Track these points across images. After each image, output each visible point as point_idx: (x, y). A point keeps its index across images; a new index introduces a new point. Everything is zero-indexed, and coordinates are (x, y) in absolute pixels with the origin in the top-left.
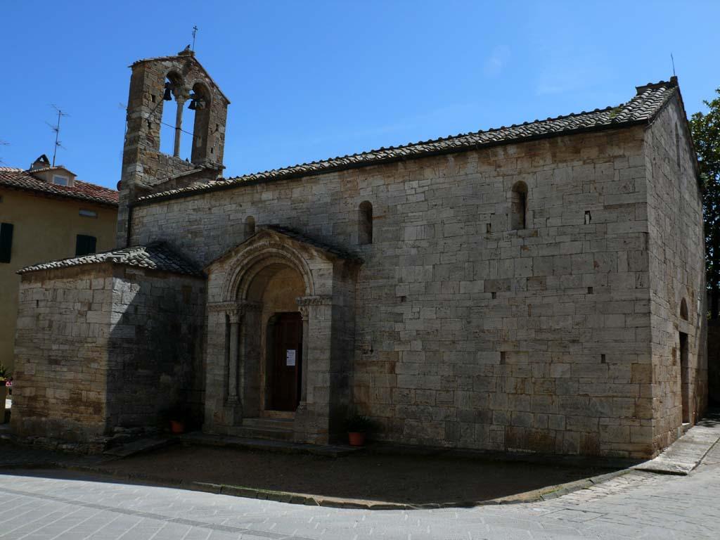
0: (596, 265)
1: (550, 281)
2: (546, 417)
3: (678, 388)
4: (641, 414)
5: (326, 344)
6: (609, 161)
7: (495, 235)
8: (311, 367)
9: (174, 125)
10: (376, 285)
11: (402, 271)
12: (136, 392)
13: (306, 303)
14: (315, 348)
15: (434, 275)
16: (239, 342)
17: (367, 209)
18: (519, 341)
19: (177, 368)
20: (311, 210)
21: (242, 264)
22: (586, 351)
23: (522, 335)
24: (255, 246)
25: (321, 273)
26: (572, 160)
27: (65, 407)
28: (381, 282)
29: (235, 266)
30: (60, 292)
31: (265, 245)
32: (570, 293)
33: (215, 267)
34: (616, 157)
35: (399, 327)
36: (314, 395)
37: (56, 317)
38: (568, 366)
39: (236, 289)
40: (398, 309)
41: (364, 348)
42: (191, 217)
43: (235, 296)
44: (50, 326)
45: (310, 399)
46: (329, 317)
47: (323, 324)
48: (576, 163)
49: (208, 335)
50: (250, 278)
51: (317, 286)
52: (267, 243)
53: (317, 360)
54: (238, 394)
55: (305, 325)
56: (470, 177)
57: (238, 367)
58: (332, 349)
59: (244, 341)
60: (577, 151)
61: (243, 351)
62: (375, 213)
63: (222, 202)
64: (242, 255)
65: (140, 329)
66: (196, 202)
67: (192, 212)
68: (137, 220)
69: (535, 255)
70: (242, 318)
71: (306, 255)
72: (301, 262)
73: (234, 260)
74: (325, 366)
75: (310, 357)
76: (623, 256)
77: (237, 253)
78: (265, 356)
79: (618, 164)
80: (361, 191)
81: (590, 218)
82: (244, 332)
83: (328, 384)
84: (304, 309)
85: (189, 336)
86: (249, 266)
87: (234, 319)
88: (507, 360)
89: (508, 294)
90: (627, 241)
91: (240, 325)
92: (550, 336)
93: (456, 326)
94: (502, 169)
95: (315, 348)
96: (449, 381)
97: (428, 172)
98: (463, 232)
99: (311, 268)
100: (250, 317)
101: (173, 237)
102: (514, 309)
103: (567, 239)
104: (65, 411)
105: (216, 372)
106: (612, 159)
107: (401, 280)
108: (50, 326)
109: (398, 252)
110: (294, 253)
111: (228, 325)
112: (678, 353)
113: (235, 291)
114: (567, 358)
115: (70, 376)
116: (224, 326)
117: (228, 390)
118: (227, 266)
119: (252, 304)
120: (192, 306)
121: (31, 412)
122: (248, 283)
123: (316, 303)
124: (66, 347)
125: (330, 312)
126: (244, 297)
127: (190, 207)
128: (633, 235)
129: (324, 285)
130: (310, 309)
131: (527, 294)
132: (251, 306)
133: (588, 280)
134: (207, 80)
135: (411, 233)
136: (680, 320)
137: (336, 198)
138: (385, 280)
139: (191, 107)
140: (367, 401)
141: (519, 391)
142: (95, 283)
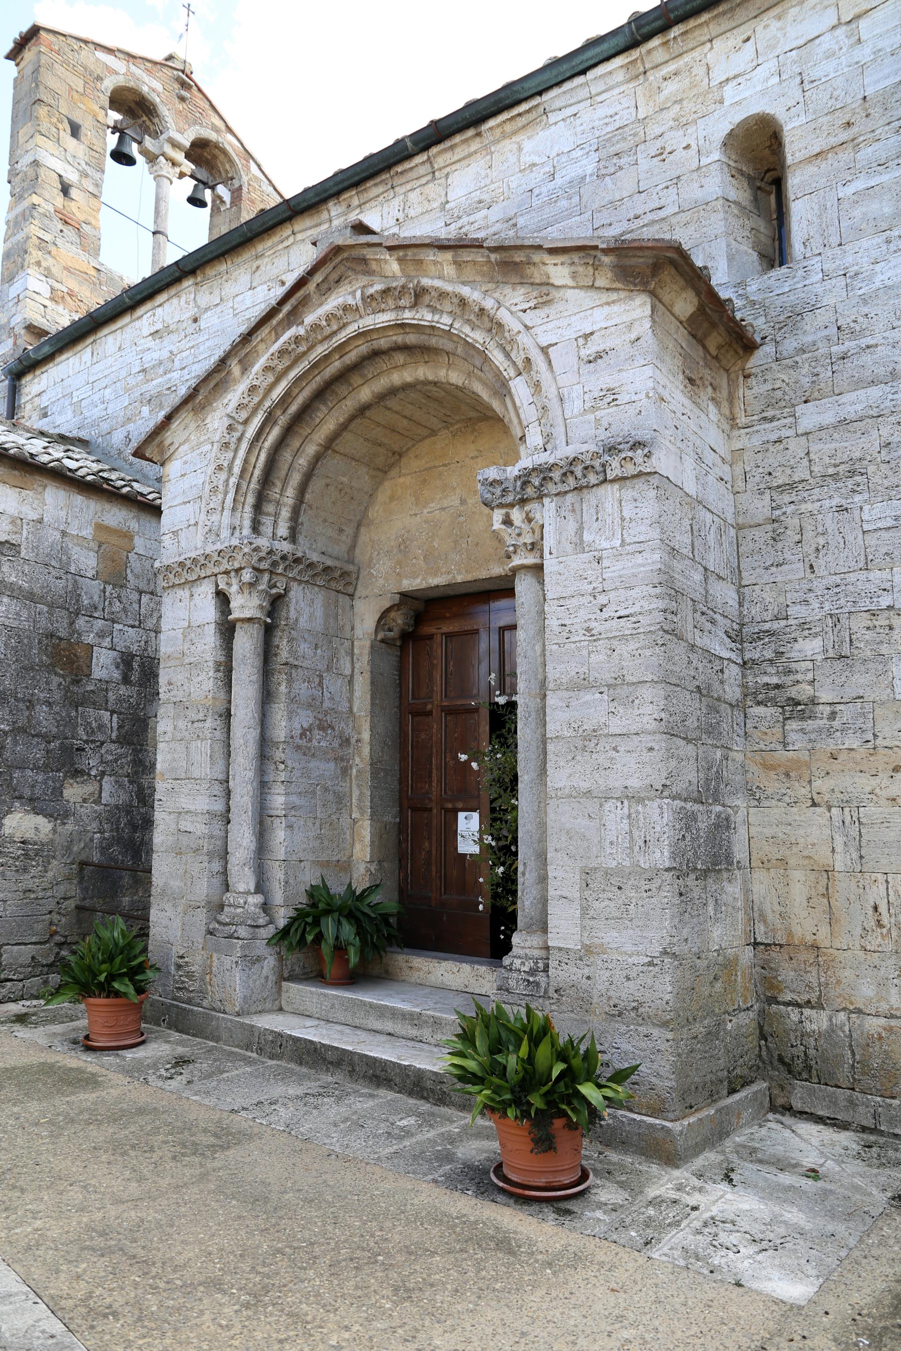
5: (638, 660)
8: (560, 777)
10: (829, 418)
13: (534, 485)
14: (583, 684)
16: (266, 696)
19: (73, 792)
20: (521, 221)
21: (267, 404)
24: (309, 319)
25: (590, 350)
29: (244, 415)
31: (346, 308)
33: (175, 434)
36: (584, 910)
39: (251, 500)
41: (793, 692)
42: (147, 357)
43: (247, 523)
45: (565, 928)
46: (643, 531)
47: (614, 569)
49: (161, 672)
50: (303, 462)
51: (574, 406)
52: (355, 300)
53: (595, 735)
54: (260, 888)
57: (263, 786)
58: (668, 682)
59: (283, 688)
61: (281, 729)
63: (230, 289)
64: (267, 369)
66: (159, 311)
67: (150, 343)
68: (29, 407)
70: (276, 603)
72: (496, 327)
73: (234, 396)
74: (635, 768)
75: (558, 721)
78: (366, 751)
80: (728, 89)
82: (284, 654)
84: (517, 515)
85: (123, 690)
86: (293, 408)
87: (245, 605)
95: (583, 684)
99: (544, 341)
100: (305, 606)
101: (105, 427)
105: (185, 803)
110: (463, 302)
111: (227, 630)
113: (248, 509)
116: (211, 630)
117: (225, 873)
118: (216, 420)
119: (314, 557)
120: (135, 596)
122: (296, 479)
123: (577, 477)
126: (283, 530)
127: (146, 332)
129: (611, 396)
130: (547, 512)
132: (311, 565)
134: (230, 137)
137: (613, 152)
138: (875, 392)
140: (823, 937)
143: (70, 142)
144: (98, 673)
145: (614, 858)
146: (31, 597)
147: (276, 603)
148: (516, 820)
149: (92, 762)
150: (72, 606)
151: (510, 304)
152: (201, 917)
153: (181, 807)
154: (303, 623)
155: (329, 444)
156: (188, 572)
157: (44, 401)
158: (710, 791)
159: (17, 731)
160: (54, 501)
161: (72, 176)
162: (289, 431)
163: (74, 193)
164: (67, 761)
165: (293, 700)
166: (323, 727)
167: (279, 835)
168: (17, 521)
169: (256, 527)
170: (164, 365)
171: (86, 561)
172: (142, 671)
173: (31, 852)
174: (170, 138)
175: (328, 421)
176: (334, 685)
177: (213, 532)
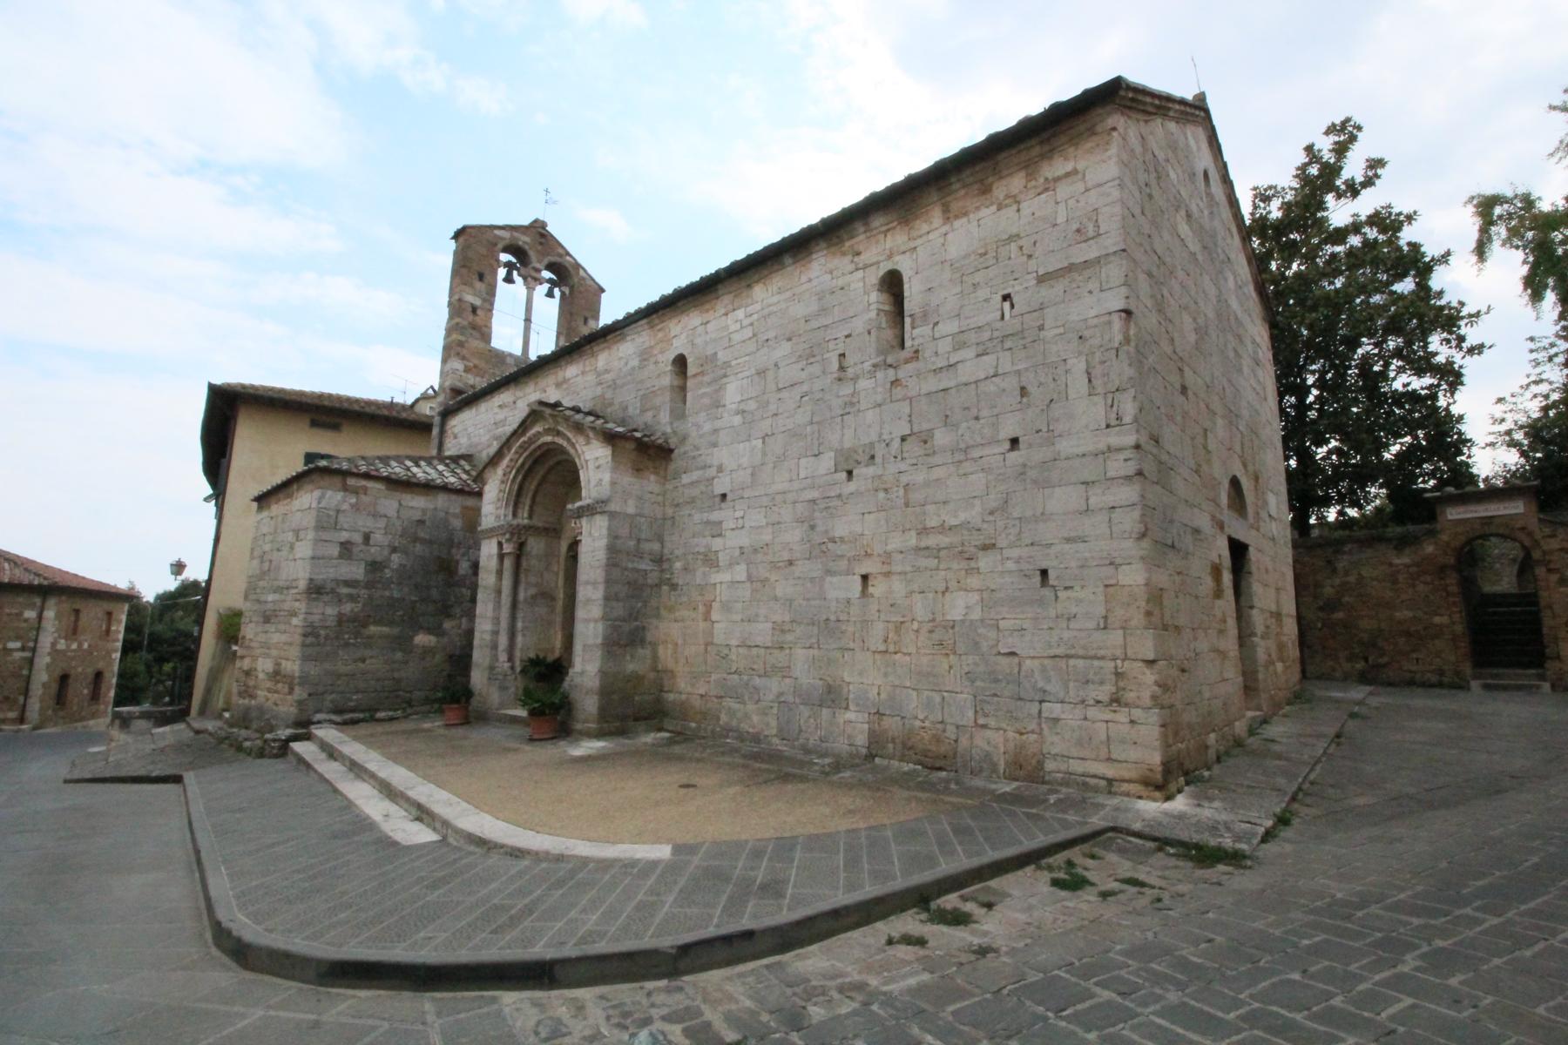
0: (1023, 391)
1: (941, 438)
2: (938, 699)
3: (1230, 644)
4: (1130, 696)
6: (1046, 190)
7: (850, 372)
11: (721, 456)
12: (363, 661)
14: (587, 583)
15: (764, 454)
17: (681, 362)
18: (888, 554)
19: (447, 625)
22: (1010, 565)
23: (895, 543)
26: (978, 208)
28: (695, 475)
32: (976, 453)
34: (1057, 179)
35: (717, 544)
38: (975, 597)
40: (715, 516)
46: (605, 532)
48: (985, 212)
56: (815, 283)
57: (513, 618)
58: (608, 582)
60: (986, 190)
62: (691, 370)
65: (375, 566)
69: (913, 393)
70: (521, 546)
71: (581, 440)
73: (505, 462)
74: (596, 611)
76: (1078, 365)
77: (509, 449)
79: (1063, 190)
81: (1012, 306)
83: (599, 641)
87: (508, 548)
88: (871, 590)
89: (871, 471)
90: (1086, 333)
92: (944, 540)
93: (794, 535)
94: (862, 257)
95: (587, 583)
96: (783, 631)
97: (759, 291)
98: (804, 375)
100: (535, 545)
102: (881, 495)
103: (969, 353)
106: (1050, 185)
107: (720, 469)
109: (718, 424)
111: (501, 557)
112: (1227, 578)
114: (974, 581)
118: (500, 471)
125: (606, 524)
128: (1095, 321)
130: (584, 521)
131: (903, 466)
133: (1008, 429)
135: (733, 393)
136: (1228, 516)
137: (645, 356)
138: (700, 472)
139: (550, 294)
141: (891, 649)
143: (478, 285)
145: (590, 641)
146: (431, 542)
147: (521, 546)
150: (450, 543)
151: (579, 441)
152: (486, 674)
154: (534, 552)
156: (491, 533)
157: (456, 430)
158: (633, 615)
159: (422, 600)
160: (441, 500)
161: (478, 302)
162: (524, 478)
164: (445, 611)
165: (528, 583)
167: (519, 639)
168: (424, 511)
169: (515, 515)
170: (503, 422)
171: (457, 523)
172: (475, 566)
173: (427, 651)
175: (541, 471)
177: (498, 517)
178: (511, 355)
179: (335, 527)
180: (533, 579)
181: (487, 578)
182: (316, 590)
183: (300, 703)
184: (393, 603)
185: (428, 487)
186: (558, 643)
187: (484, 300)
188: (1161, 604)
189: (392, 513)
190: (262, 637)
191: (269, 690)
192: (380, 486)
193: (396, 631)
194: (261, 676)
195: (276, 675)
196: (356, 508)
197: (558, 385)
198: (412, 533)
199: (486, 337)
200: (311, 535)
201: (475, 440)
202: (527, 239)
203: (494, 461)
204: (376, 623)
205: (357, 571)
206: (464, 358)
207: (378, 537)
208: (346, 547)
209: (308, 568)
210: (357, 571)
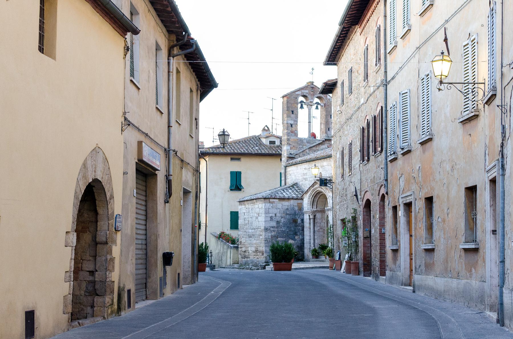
9: (308, 121)
19: (296, 237)
27: (254, 254)
30: (250, 209)
37: (250, 219)
44: (248, 223)
55: (73, 258)
57: (314, 236)
61: (316, 229)
65: (278, 222)
70: (315, 216)
73: (309, 193)
87: (311, 217)
91: (314, 219)
100: (318, 215)
104: (254, 255)
108: (248, 223)
111: (310, 219)
115: (255, 242)
121: (245, 257)
124: (253, 231)
142: (260, 205)
144: (299, 222)
147: (315, 216)
148: (297, 130)
149: (298, 234)
153: (307, 238)
155: (319, 198)
156: (306, 212)
157: (290, 172)
160: (292, 202)
161: (292, 122)
163: (293, 126)
164: (296, 234)
166: (321, 229)
167: (316, 241)
168: (288, 206)
169: (312, 207)
171: (296, 208)
172: (302, 220)
174: (232, 228)
176: (322, 224)
178: (305, 139)
179: (269, 213)
180: (318, 225)
181: (306, 224)
182: (266, 229)
183: (266, 257)
184: (283, 232)
185: (289, 199)
186: (326, 242)
187: (295, 121)
188: (95, 259)
189: (280, 207)
190: (249, 242)
191: (254, 255)
192: (277, 200)
193: (284, 239)
194: (250, 252)
195: (256, 251)
196: (272, 207)
197: (322, 167)
198: (286, 212)
199: (296, 135)
200: (263, 215)
201: (298, 178)
202: (307, 91)
203: (307, 191)
204: (280, 237)
205: (274, 224)
206: (290, 144)
207: (278, 215)
208: (271, 217)
209: (264, 224)
210: (274, 224)
